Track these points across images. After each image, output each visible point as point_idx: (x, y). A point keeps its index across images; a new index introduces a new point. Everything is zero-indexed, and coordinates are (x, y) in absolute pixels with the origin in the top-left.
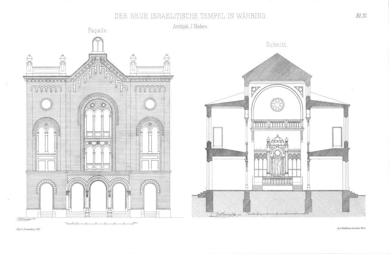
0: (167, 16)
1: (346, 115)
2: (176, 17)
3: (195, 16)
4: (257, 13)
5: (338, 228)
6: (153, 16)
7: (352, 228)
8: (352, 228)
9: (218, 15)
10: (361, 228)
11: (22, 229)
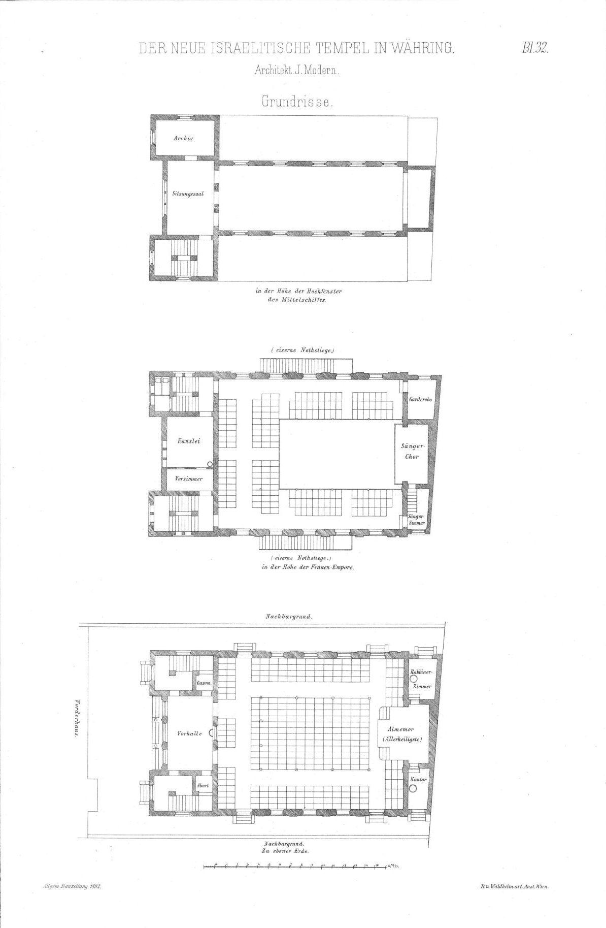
0: (236, 49)
1: (152, 268)
2: (264, 50)
3: (303, 48)
4: (435, 41)
5: (483, 886)
6: (216, 48)
7: (516, 887)
8: (516, 887)
9: (354, 44)
10: (538, 886)
11: (57, 886)
